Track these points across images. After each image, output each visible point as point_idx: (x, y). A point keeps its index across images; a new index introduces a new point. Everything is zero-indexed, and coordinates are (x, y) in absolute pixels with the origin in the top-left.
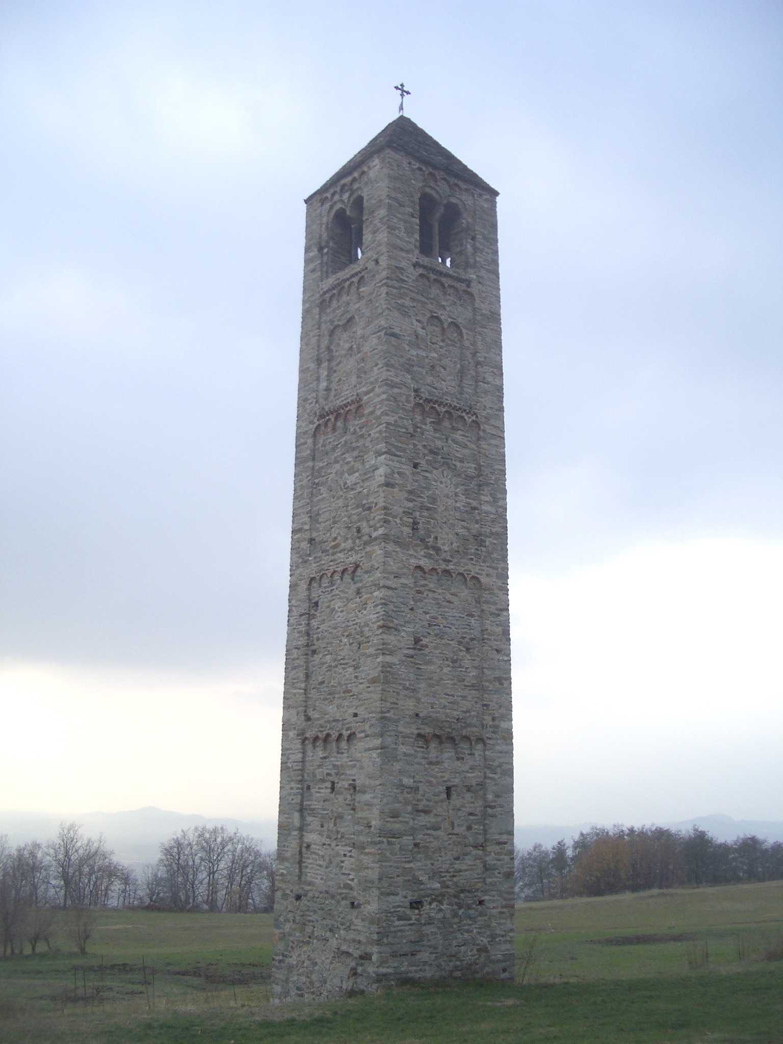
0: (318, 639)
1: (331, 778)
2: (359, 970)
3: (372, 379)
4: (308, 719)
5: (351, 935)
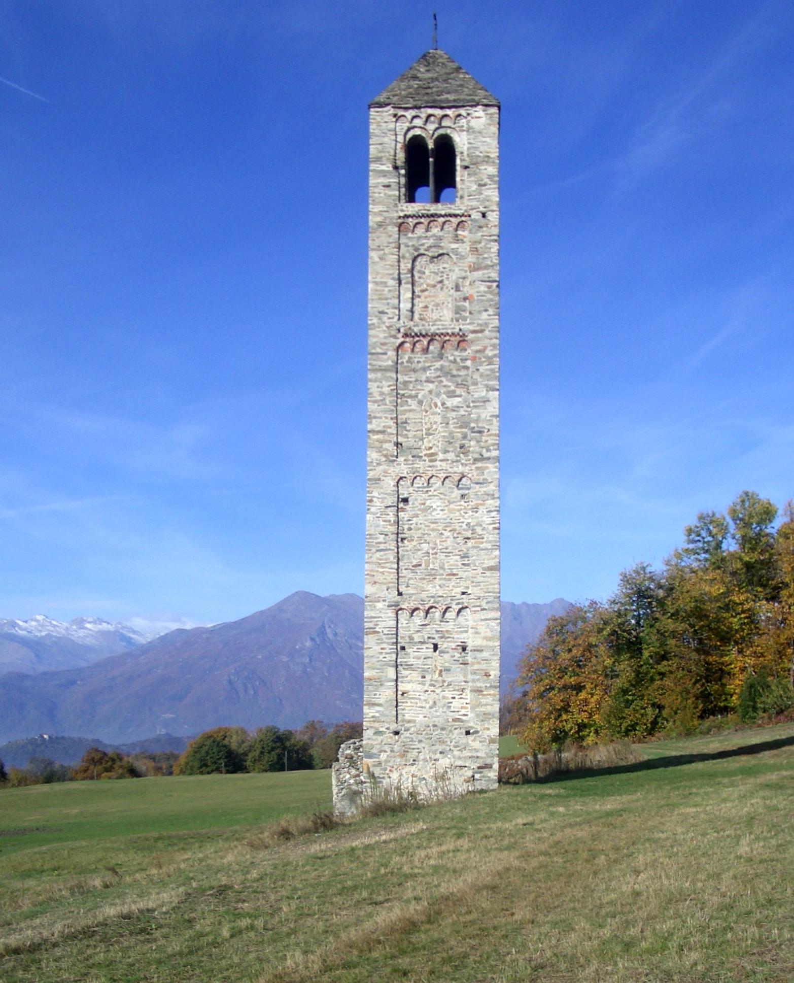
0: (410, 529)
1: (434, 641)
2: (477, 776)
3: (480, 322)
4: (400, 594)
5: (466, 753)
